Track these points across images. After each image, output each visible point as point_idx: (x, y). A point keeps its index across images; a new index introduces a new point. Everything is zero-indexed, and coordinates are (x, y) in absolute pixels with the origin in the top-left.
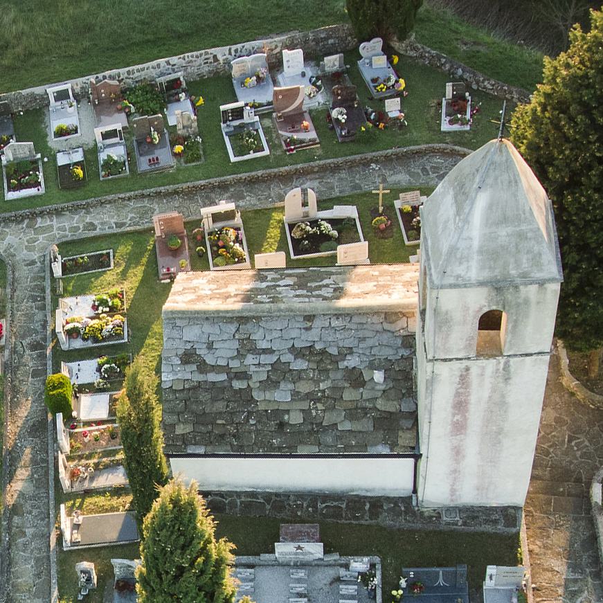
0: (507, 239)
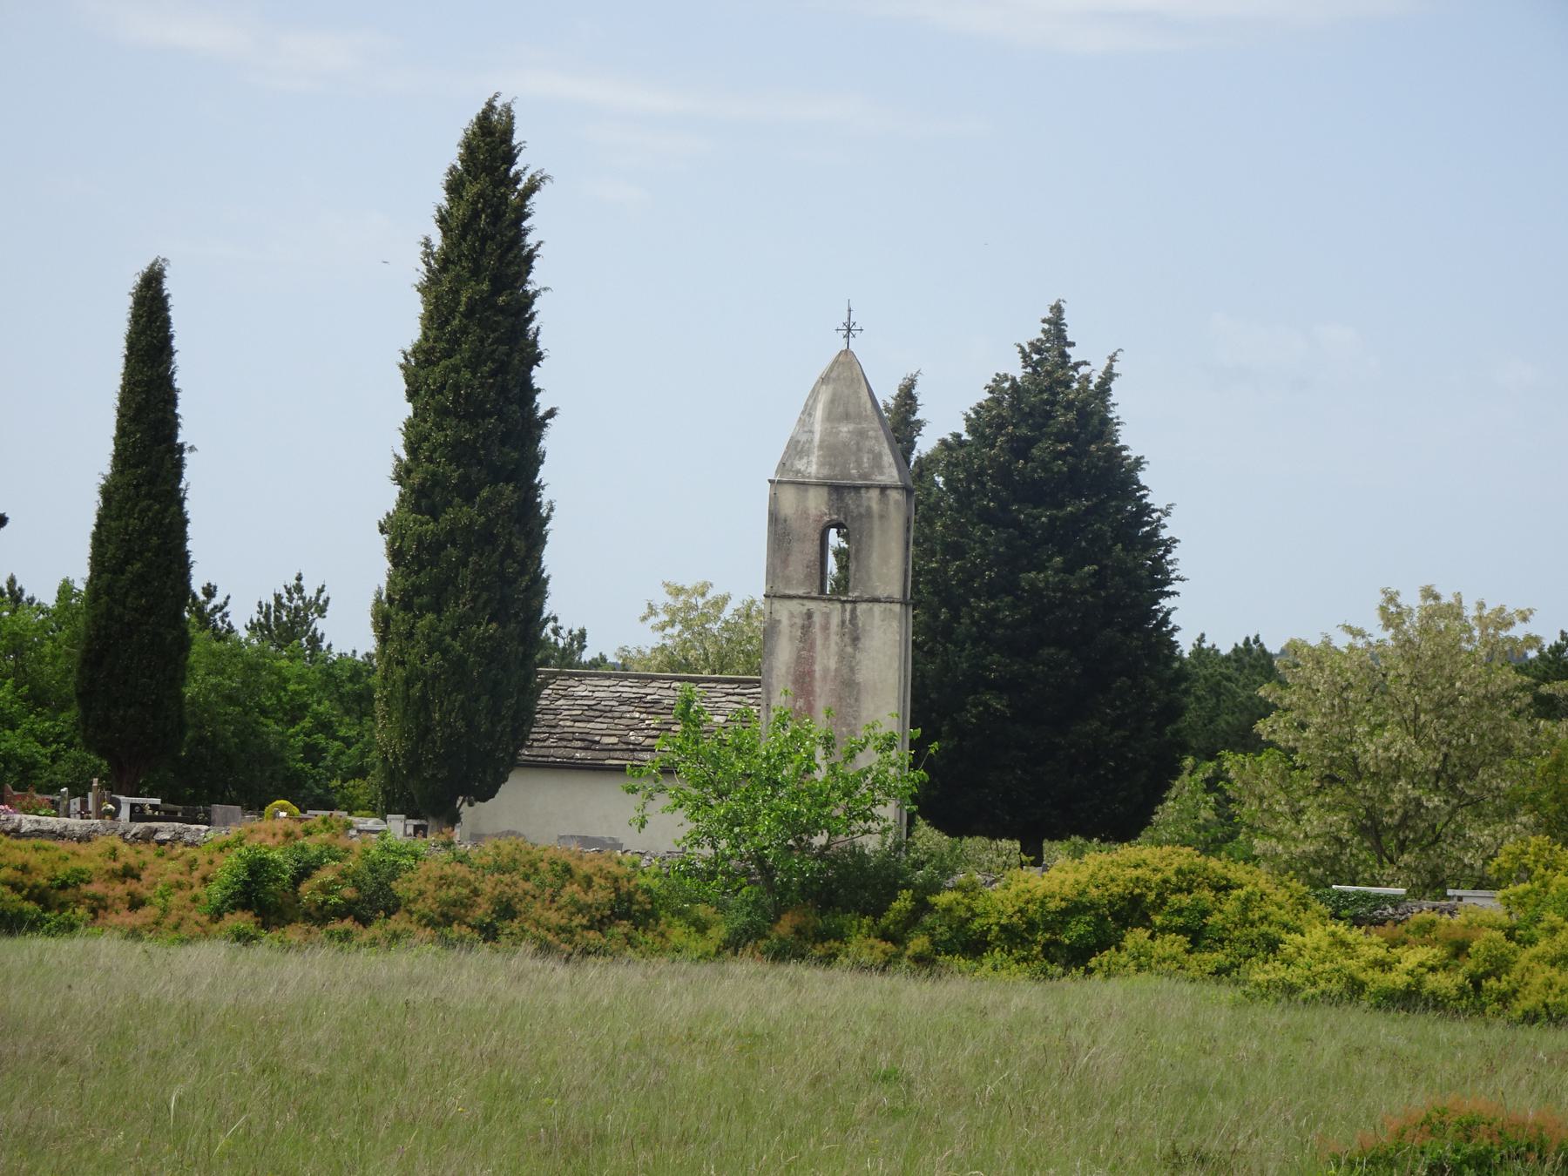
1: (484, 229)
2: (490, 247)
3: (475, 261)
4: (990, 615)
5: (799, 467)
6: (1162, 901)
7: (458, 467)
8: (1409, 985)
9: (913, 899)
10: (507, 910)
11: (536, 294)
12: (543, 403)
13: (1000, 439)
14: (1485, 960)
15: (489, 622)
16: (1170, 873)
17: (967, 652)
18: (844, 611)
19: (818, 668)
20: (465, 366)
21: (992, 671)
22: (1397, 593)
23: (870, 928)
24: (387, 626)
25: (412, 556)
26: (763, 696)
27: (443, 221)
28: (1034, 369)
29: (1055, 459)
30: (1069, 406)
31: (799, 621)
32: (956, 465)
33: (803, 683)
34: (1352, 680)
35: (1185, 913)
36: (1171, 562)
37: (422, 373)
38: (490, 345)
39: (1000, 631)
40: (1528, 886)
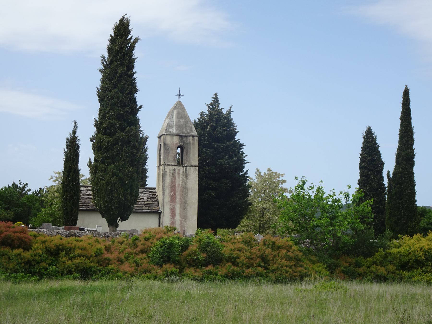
0: (183, 123)
1: (124, 52)
5: (171, 131)
17: (204, 180)
18: (183, 169)
19: (177, 184)
21: (211, 185)
25: (105, 148)
31: (172, 172)
33: (173, 188)
38: (127, 86)
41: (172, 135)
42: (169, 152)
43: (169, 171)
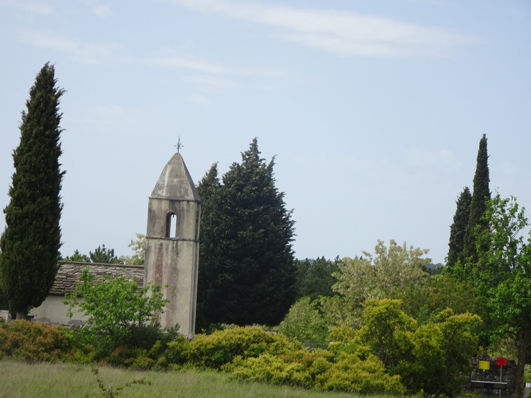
1: (42, 108)
2: (44, 114)
3: (39, 119)
4: (227, 246)
6: (248, 346)
7: (30, 191)
8: (287, 376)
9: (161, 343)
10: (16, 344)
11: (61, 131)
12: (61, 169)
13: (233, 185)
14: (317, 368)
15: (39, 245)
16: (251, 337)
18: (173, 244)
19: (164, 263)
20: (34, 156)
21: (228, 265)
22: (383, 242)
23: (146, 354)
24: (4, 246)
26: (145, 273)
27: (28, 105)
28: (247, 161)
29: (252, 192)
30: (257, 174)
31: (158, 247)
32: (218, 194)
34: (364, 271)
35: (255, 351)
36: (293, 229)
37: (19, 158)
39: (230, 252)
40: (340, 342)
41: (160, 199)
42: (155, 222)
43: (155, 246)
